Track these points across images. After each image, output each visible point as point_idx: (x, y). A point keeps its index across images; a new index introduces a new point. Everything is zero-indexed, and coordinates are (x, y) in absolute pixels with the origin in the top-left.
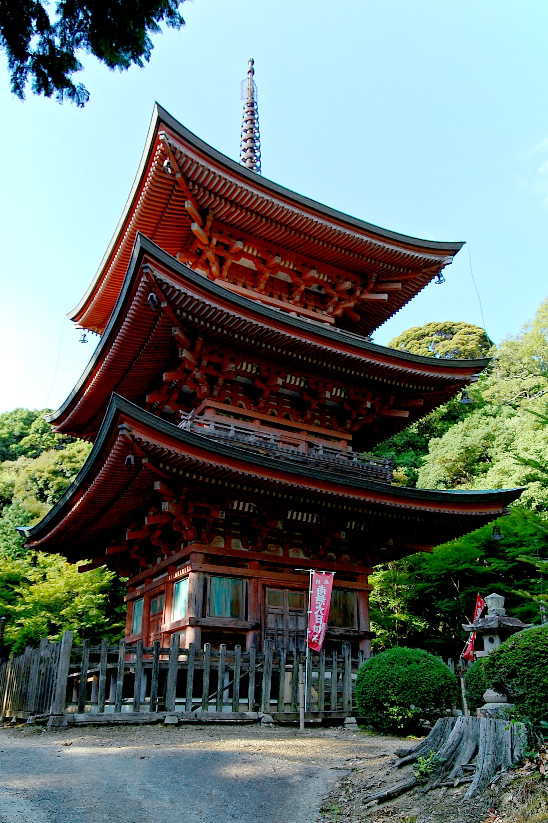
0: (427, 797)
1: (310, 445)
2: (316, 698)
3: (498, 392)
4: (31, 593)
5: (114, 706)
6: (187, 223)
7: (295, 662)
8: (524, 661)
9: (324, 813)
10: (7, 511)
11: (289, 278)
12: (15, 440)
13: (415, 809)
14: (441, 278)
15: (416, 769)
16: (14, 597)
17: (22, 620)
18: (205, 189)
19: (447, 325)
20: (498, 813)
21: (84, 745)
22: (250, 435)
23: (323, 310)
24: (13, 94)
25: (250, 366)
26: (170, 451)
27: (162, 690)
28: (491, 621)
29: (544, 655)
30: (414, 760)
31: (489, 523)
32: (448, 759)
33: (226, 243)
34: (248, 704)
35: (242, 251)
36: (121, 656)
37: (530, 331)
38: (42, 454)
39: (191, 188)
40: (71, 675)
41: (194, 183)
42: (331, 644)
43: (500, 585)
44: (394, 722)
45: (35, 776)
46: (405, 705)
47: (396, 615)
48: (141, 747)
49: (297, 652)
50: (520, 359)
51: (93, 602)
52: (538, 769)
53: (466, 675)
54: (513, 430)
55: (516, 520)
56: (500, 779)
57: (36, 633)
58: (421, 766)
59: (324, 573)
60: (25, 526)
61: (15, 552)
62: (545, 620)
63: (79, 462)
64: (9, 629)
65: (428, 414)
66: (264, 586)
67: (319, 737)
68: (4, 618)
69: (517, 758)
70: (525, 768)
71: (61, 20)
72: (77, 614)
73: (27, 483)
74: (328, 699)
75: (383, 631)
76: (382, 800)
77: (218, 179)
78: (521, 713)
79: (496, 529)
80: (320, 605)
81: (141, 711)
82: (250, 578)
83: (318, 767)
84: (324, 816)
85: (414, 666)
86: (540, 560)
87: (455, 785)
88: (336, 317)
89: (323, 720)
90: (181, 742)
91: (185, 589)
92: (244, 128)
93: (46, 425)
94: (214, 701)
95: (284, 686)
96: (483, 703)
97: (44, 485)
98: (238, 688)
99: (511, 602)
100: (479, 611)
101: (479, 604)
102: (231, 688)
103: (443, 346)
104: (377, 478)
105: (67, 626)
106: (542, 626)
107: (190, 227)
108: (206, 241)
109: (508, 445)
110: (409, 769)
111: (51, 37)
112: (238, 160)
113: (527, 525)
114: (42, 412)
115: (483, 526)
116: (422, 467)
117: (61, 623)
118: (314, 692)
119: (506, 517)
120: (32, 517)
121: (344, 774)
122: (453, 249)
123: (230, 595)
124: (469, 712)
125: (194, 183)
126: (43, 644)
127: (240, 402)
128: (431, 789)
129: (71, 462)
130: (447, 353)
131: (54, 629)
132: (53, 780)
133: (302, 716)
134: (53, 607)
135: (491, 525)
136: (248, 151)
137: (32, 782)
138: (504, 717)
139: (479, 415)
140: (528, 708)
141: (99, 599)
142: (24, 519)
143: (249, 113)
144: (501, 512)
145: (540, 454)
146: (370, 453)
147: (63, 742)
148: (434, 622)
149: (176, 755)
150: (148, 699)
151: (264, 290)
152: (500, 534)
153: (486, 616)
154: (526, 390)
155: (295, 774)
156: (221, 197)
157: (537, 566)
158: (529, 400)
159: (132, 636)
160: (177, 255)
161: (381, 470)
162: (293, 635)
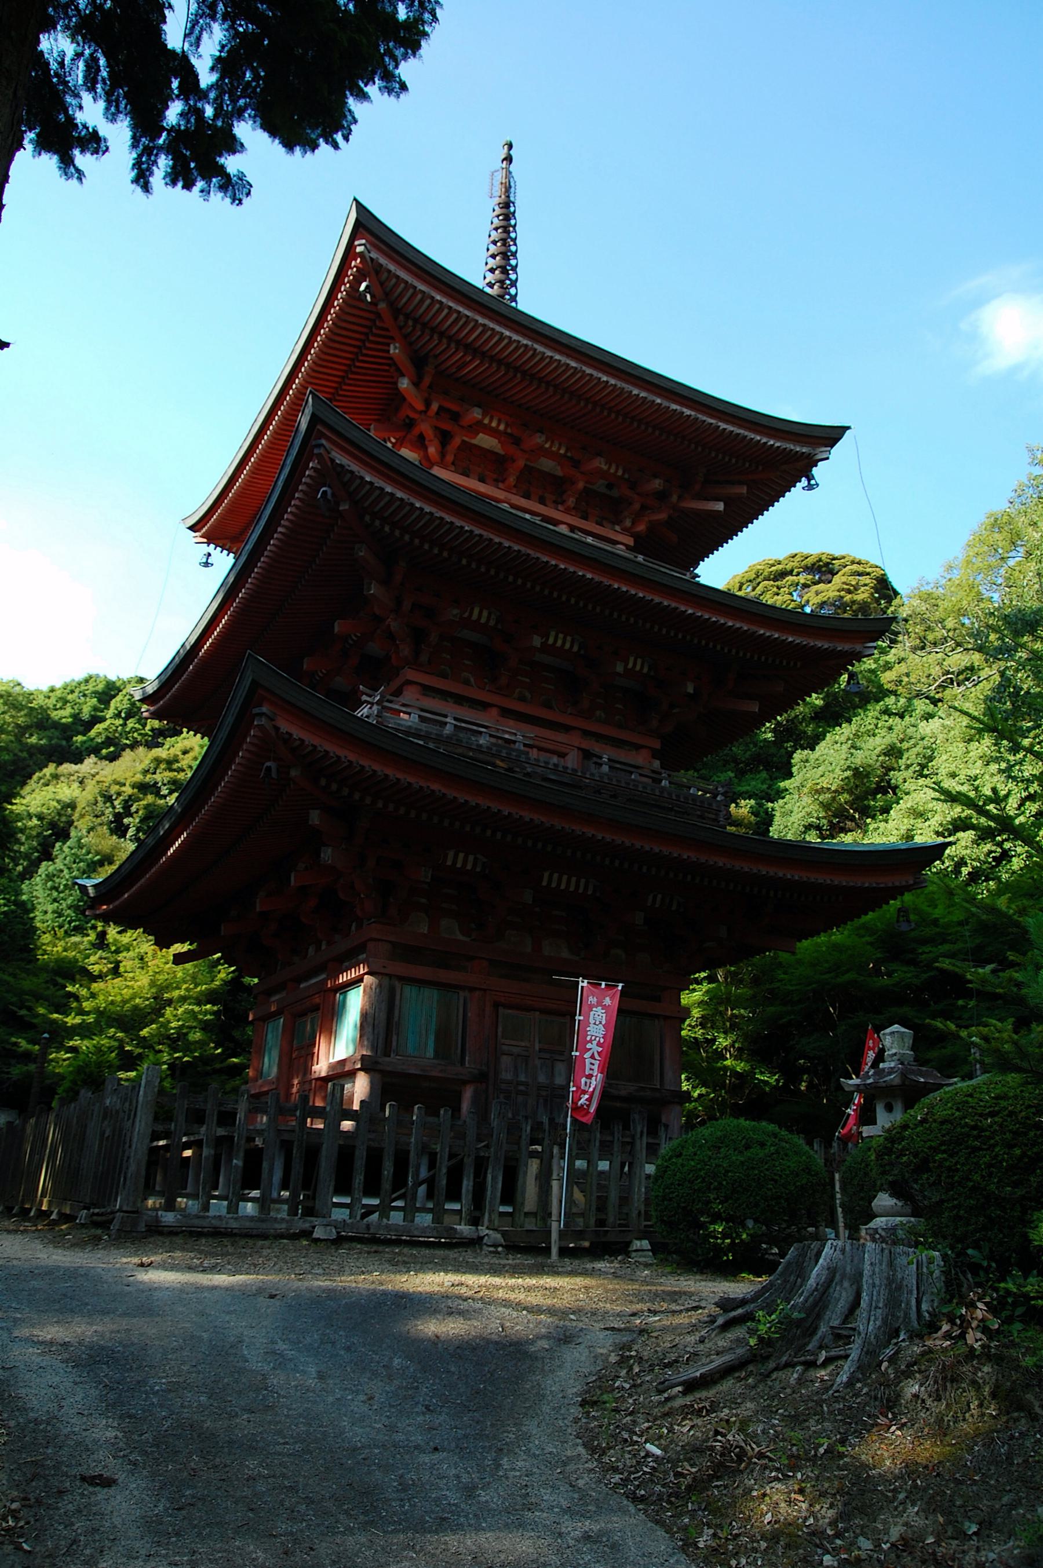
0: (769, 1383)
1: (587, 755)
2: (582, 1206)
3: (907, 675)
4: (93, 996)
5: (225, 1203)
6: (392, 377)
7: (546, 1142)
8: (943, 1143)
9: (587, 1408)
10: (61, 849)
11: (559, 468)
12: (81, 729)
13: (749, 1405)
14: (813, 482)
15: (752, 1332)
16: (64, 1001)
17: (76, 1042)
18: (424, 325)
19: (824, 558)
20: (895, 1418)
21: (173, 1268)
22: (481, 733)
23: (614, 523)
24: (134, 186)
25: (485, 613)
26: (339, 757)
27: (309, 1181)
28: (890, 1074)
29: (975, 1132)
30: (749, 1317)
31: (892, 902)
32: (808, 1316)
33: (454, 408)
34: (459, 1212)
35: (480, 422)
36: (240, 1116)
37: (956, 575)
38: (124, 753)
39: (402, 324)
40: (155, 1144)
41: (407, 316)
42: (613, 1108)
43: (906, 1010)
44: (718, 1250)
45: (86, 1319)
46: (735, 1221)
47: (728, 1063)
48: (270, 1277)
49: (550, 1124)
50: (942, 621)
51: (195, 1018)
52: (962, 1336)
53: (843, 1168)
54: (932, 740)
55: (936, 896)
56: (897, 1353)
57: (99, 1065)
58: (761, 1327)
59: (603, 986)
60: (89, 877)
61: (70, 923)
62: (978, 1073)
63: (184, 770)
64: (54, 1055)
65: (793, 709)
66: (497, 1005)
67: (585, 1273)
68: (46, 1035)
69: (927, 1315)
70: (940, 1333)
71: (217, 81)
72: (168, 1037)
73: (96, 802)
74: (602, 1205)
75: (704, 1090)
76: (691, 1386)
77: (446, 311)
78: (935, 1235)
79: (902, 911)
80: (595, 1043)
81: (272, 1214)
82: (472, 989)
83: (580, 1325)
84: (588, 1413)
85: (757, 1152)
86: (974, 967)
87: (819, 1362)
88: (636, 537)
89: (591, 1243)
90: (341, 1272)
91: (355, 1002)
92: (492, 239)
93: (133, 704)
94: (399, 1203)
95: (525, 1183)
96: (873, 1216)
97: (123, 808)
98: (444, 1182)
99: (924, 1041)
100: (871, 1055)
101: (871, 1045)
102: (431, 1182)
103: (817, 593)
104: (702, 817)
105: (151, 1057)
106: (974, 1082)
107: (396, 383)
108: (420, 406)
109: (923, 766)
110: (739, 1332)
111: (199, 105)
112: (480, 284)
113: (953, 906)
114: (129, 682)
115: (881, 907)
116: (781, 801)
117: (141, 1051)
118: (578, 1195)
119: (919, 891)
120: (101, 863)
121: (626, 1338)
122: (831, 436)
123: (434, 1019)
124: (847, 1232)
125: (407, 316)
126: (109, 1087)
127: (466, 674)
128: (777, 1369)
129: (171, 770)
130: (822, 605)
131: (129, 1061)
132: (115, 1327)
133: (554, 1236)
134: (129, 1020)
135: (894, 904)
136: (497, 272)
137: (79, 1330)
138: (906, 1242)
139: (876, 714)
140: (947, 1226)
141: (206, 1013)
142: (88, 865)
143: (501, 218)
144: (911, 882)
145: (976, 783)
146: (691, 772)
147: (136, 1260)
148: (791, 1074)
149: (331, 1294)
150: (285, 1194)
151: (515, 486)
152: (908, 921)
153: (881, 1065)
154: (953, 673)
155: (539, 1337)
156: (450, 339)
157: (969, 977)
158: (958, 690)
159: (260, 1082)
160: (372, 427)
161: (710, 804)
162: (544, 1093)
